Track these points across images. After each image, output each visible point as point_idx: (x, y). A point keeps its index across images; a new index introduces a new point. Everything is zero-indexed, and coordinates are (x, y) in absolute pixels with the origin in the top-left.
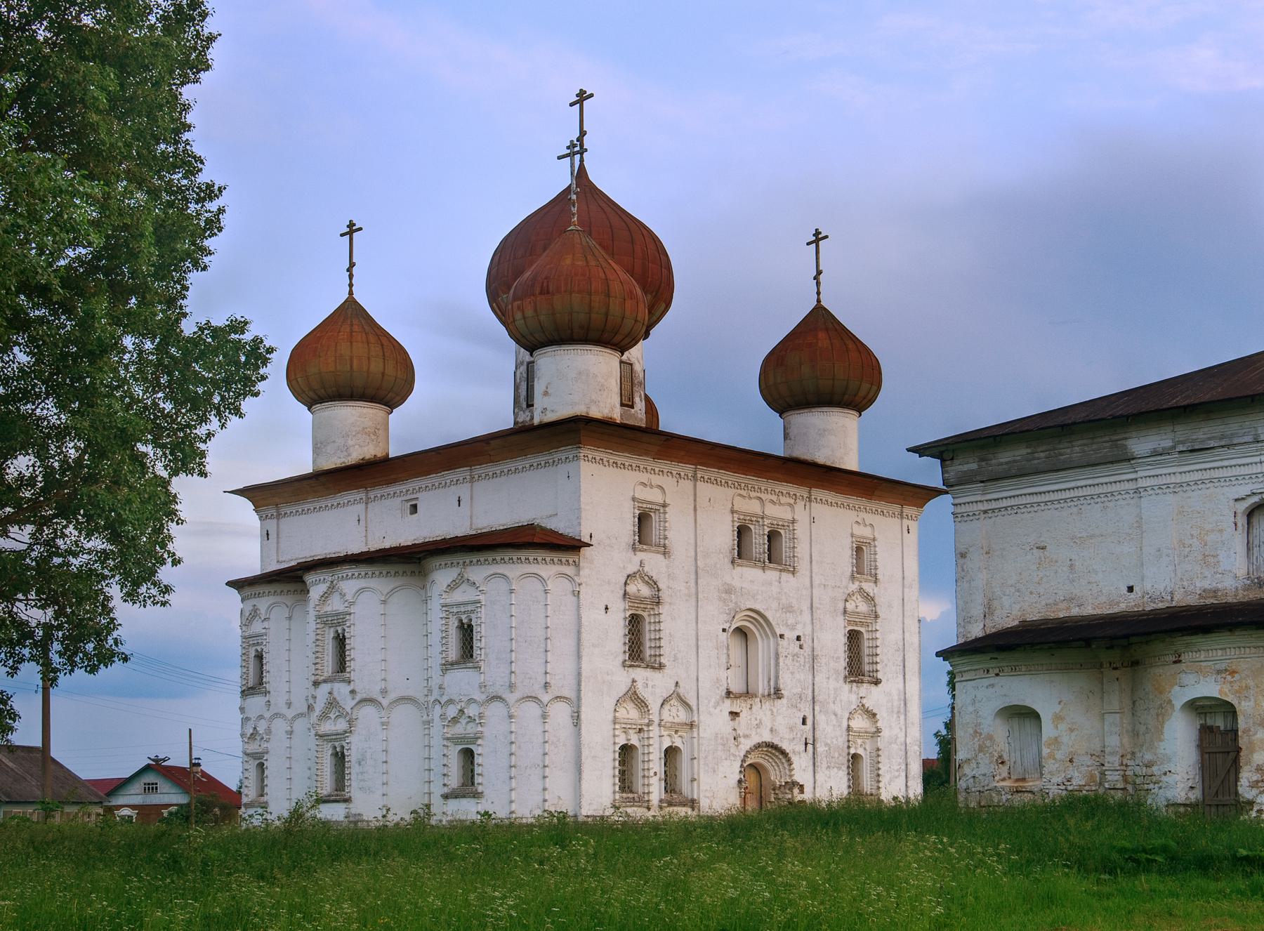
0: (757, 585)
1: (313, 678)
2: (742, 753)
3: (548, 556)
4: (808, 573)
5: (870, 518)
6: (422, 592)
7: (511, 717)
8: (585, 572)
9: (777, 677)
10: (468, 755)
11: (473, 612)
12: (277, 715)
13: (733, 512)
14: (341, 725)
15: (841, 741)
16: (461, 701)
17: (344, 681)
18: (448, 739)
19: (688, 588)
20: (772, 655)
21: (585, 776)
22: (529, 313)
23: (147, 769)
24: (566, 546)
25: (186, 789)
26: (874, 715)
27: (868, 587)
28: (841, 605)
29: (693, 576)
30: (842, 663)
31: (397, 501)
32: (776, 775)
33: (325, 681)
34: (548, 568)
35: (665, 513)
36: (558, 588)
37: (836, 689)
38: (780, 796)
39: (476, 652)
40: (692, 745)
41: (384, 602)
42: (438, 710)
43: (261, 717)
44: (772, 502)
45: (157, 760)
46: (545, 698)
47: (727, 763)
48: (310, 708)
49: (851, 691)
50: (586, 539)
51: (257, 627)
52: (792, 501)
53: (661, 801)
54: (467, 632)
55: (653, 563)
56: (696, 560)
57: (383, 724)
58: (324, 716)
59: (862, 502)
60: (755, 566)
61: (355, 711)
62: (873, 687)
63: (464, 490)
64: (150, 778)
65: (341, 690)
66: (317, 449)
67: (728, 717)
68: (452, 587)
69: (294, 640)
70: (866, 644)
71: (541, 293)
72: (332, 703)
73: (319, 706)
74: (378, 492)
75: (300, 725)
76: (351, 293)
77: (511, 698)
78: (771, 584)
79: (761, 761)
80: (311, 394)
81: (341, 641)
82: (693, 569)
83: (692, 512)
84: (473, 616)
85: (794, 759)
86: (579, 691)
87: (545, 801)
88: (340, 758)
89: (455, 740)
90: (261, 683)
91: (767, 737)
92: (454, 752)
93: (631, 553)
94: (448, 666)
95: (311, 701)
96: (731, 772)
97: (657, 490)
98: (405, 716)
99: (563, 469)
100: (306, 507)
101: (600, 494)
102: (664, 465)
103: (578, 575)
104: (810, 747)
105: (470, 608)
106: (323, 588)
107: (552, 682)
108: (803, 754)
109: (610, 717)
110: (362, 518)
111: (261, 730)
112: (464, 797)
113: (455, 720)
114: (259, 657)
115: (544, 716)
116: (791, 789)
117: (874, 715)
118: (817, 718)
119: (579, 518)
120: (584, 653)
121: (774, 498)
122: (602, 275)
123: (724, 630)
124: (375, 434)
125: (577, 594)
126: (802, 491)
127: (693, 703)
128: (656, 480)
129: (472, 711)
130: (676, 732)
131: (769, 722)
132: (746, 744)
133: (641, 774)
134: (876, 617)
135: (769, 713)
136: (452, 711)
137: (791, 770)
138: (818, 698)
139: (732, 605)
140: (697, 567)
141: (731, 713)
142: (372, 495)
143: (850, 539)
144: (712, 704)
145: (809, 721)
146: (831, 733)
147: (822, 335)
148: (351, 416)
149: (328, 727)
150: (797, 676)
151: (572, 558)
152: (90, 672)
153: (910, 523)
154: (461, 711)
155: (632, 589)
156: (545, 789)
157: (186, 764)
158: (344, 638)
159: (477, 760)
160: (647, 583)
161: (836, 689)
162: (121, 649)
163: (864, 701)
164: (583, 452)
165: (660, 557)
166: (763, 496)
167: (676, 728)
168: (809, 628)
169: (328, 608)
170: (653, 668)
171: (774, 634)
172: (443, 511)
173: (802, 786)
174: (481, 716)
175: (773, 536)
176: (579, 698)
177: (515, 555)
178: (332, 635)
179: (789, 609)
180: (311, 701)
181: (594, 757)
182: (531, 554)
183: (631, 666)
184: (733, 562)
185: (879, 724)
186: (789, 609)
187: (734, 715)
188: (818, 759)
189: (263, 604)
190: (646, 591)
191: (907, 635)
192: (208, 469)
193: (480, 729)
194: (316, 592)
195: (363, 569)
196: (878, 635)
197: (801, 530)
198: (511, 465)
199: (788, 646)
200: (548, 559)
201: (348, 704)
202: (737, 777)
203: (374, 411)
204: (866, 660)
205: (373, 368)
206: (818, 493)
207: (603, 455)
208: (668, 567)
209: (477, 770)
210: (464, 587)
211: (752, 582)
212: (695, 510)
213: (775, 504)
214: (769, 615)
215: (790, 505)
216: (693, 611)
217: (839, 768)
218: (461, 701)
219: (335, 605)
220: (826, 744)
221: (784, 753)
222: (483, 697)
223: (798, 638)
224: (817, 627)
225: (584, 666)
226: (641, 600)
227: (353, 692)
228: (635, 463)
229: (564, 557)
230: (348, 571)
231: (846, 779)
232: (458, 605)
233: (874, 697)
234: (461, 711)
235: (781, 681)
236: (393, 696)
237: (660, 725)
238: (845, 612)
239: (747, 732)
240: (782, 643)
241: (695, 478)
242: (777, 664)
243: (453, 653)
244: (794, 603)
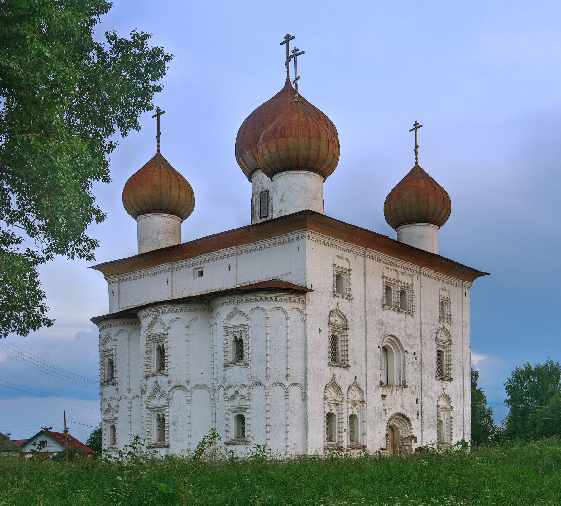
1: (145, 374)
2: (388, 419)
3: (288, 296)
4: (419, 316)
5: (448, 287)
6: (210, 321)
7: (267, 395)
8: (309, 308)
9: (404, 376)
10: (241, 419)
11: (243, 331)
12: (122, 397)
13: (383, 277)
14: (163, 402)
15: (434, 413)
16: (236, 386)
17: (164, 375)
18: (228, 409)
19: (361, 321)
20: (402, 363)
21: (310, 431)
22: (273, 149)
23: (41, 433)
24: (299, 291)
25: (62, 444)
26: (450, 398)
27: (447, 325)
28: (434, 335)
29: (363, 314)
30: (434, 369)
31: (191, 269)
32: (403, 432)
33: (152, 375)
34: (288, 304)
35: (350, 275)
36: (294, 316)
37: (431, 383)
38: (405, 444)
39: (245, 356)
40: (363, 413)
41: (188, 327)
42: (222, 391)
43: (113, 398)
44: (402, 273)
45: (46, 428)
46: (287, 384)
47: (380, 424)
48: (143, 392)
49: (439, 385)
50: (309, 287)
51: (110, 345)
52: (412, 274)
53: (348, 446)
54: (239, 343)
55: (344, 305)
56: (365, 304)
57: (188, 400)
58: (152, 397)
60: (394, 310)
61: (171, 393)
62: (449, 383)
63: (232, 261)
64: (43, 438)
65: (162, 380)
66: (141, 242)
67: (381, 398)
68: (230, 317)
69: (133, 353)
70: (445, 358)
71: (280, 137)
72: (157, 389)
73: (149, 391)
74: (179, 264)
75: (136, 402)
76: (159, 151)
77: (267, 384)
78: (401, 321)
79: (395, 424)
80: (138, 209)
81: (161, 352)
82: (364, 309)
83: (363, 275)
84: (243, 334)
85: (413, 423)
86: (306, 380)
87: (287, 446)
88: (162, 422)
89: (233, 410)
90: (112, 378)
91: (400, 410)
92: (232, 417)
93: (332, 298)
94: (228, 365)
95: (143, 388)
96: (383, 430)
97: (345, 261)
98: (200, 396)
99: (295, 244)
100: (135, 275)
101: (314, 260)
102: (349, 246)
103: (305, 309)
104: (420, 416)
105: (241, 329)
106: (150, 319)
107: (291, 374)
108: (417, 420)
109: (322, 396)
110: (170, 280)
111: (113, 406)
112: (239, 444)
113: (233, 398)
114: (111, 363)
115: (286, 395)
116: (411, 440)
117: (450, 398)
118: (424, 399)
119: (305, 274)
120: (309, 356)
121: (403, 271)
122: (316, 127)
123: (379, 347)
124: (174, 233)
125: (304, 321)
126: (416, 268)
127: (364, 389)
128: (346, 255)
129: (243, 392)
130: (355, 406)
131: (402, 401)
132: (390, 414)
133: (337, 430)
134: (451, 343)
135: (400, 396)
136: (231, 392)
137: (411, 429)
138: (424, 388)
139: (383, 332)
140: (365, 308)
142: (175, 266)
143: (438, 298)
144: (373, 389)
145: (419, 401)
146: (430, 409)
147: (421, 181)
148: (160, 222)
149: (154, 403)
150: (414, 375)
152: (21, 334)
153: (466, 290)
154: (237, 392)
155: (332, 319)
156: (287, 439)
157: (61, 430)
158: (163, 349)
159: (247, 421)
160: (340, 317)
161: (431, 383)
162: (47, 315)
163: (445, 390)
164: (308, 233)
165: (347, 301)
166: (399, 270)
167: (355, 404)
168: (419, 349)
169: (153, 332)
170: (344, 367)
171: (403, 350)
172: (219, 274)
173: (416, 438)
174: (249, 395)
175: (402, 293)
176: (306, 384)
177: (269, 295)
178: (156, 348)
179: (410, 336)
180: (143, 388)
181: (314, 420)
182: (279, 296)
183: (333, 366)
184: (383, 307)
185: (451, 404)
186: (410, 336)
188: (424, 423)
189: (113, 331)
190: (339, 322)
191: (464, 354)
193: (248, 402)
194: (145, 322)
196: (451, 353)
197: (416, 289)
198: (262, 244)
199: (410, 358)
200: (288, 299)
201: (167, 389)
202: (385, 432)
203: (173, 220)
204: (445, 367)
205: (173, 193)
206: (425, 270)
207: (318, 237)
208: (351, 307)
209: (247, 428)
210: (238, 316)
211: (392, 319)
212: (365, 274)
213: (405, 274)
214: (400, 339)
215: (410, 275)
216: (364, 334)
217: (433, 428)
218: (236, 386)
219: (158, 329)
220: (428, 415)
221: (408, 419)
222: (250, 383)
223: (414, 353)
224: (424, 347)
226: (338, 327)
227: (169, 381)
228: (334, 243)
229: (297, 298)
230: (165, 308)
231: (436, 434)
232: (234, 327)
234: (237, 392)
235: (406, 378)
236: (193, 384)
237: (347, 402)
238: (436, 339)
239: (390, 407)
240: (407, 356)
241: (365, 255)
242: (404, 368)
243: (231, 357)
244: (413, 333)
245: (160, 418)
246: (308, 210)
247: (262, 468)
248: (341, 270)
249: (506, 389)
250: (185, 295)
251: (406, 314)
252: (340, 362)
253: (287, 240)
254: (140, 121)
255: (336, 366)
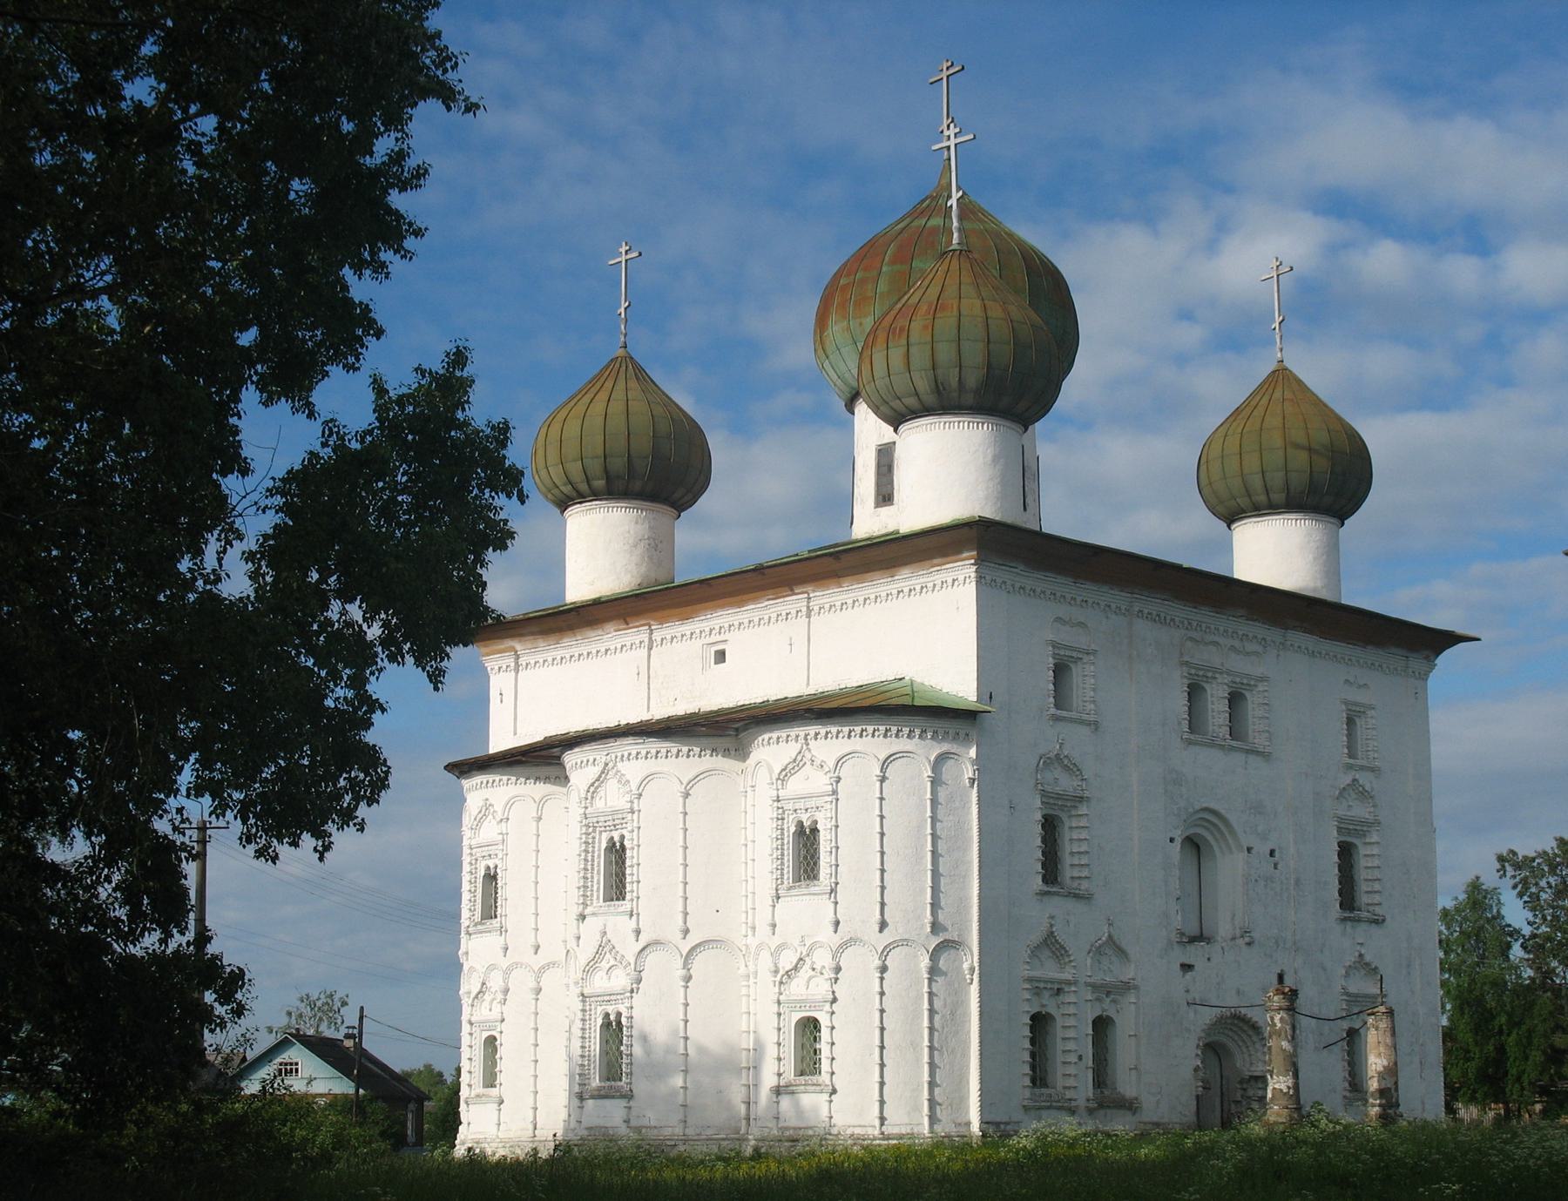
0: (1216, 775)
27: (1365, 779)
31: (697, 644)
43: (492, 968)
45: (329, 1008)
55: (1077, 742)
59: (1354, 652)
79: (1223, 1039)
95: (572, 944)
106: (593, 772)
121: (1237, 643)
131: (1235, 979)
141: (1183, 966)
151: (1416, 663)
152: (381, 784)
166: (1221, 640)
175: (1235, 699)
187: (1186, 967)
192: (420, 223)
195: (653, 745)
219: (613, 797)
223: (1272, 853)
225: (1217, 1071)
230: (628, 746)
233: (1377, 945)
245: (610, 1024)
246: (1206, 446)
247: (1040, 535)
248: (1068, 653)
249: (446, 59)
250: (681, 709)
251: (1247, 752)
252: (1068, 881)
253: (930, 585)
254: (431, 30)
255: (1055, 894)
